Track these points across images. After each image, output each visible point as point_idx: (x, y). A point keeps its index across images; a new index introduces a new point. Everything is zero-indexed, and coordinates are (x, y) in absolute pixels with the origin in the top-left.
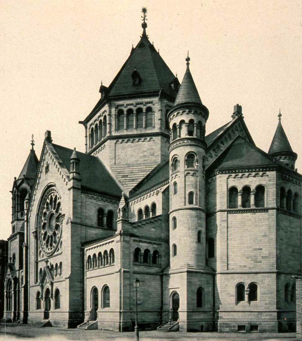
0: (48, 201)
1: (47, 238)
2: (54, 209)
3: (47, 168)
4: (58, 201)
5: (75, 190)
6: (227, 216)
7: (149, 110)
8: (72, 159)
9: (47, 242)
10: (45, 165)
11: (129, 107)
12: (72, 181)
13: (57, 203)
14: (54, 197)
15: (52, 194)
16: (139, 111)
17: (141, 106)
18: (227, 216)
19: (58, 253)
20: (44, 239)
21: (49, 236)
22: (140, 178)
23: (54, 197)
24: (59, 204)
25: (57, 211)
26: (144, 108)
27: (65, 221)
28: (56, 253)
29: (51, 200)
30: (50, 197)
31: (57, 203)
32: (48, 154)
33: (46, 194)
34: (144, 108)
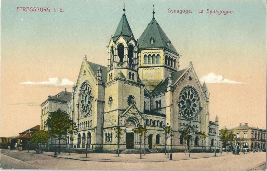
0: (85, 89)
1: (84, 107)
2: (88, 93)
3: (85, 73)
4: (90, 90)
5: (99, 85)
6: (116, 110)
7: (158, 55)
8: (169, 78)
9: (84, 109)
10: (84, 71)
11: (154, 53)
12: (98, 81)
13: (89, 91)
14: (88, 87)
15: (87, 86)
16: (150, 55)
17: (150, 54)
18: (116, 110)
19: (90, 115)
20: (82, 107)
21: (85, 107)
22: (155, 86)
23: (88, 87)
24: (91, 91)
25: (89, 95)
26: (156, 55)
27: (94, 100)
28: (88, 115)
29: (86, 89)
30: (85, 87)
31: (89, 91)
32: (85, 66)
33: (84, 86)
34: (156, 55)
